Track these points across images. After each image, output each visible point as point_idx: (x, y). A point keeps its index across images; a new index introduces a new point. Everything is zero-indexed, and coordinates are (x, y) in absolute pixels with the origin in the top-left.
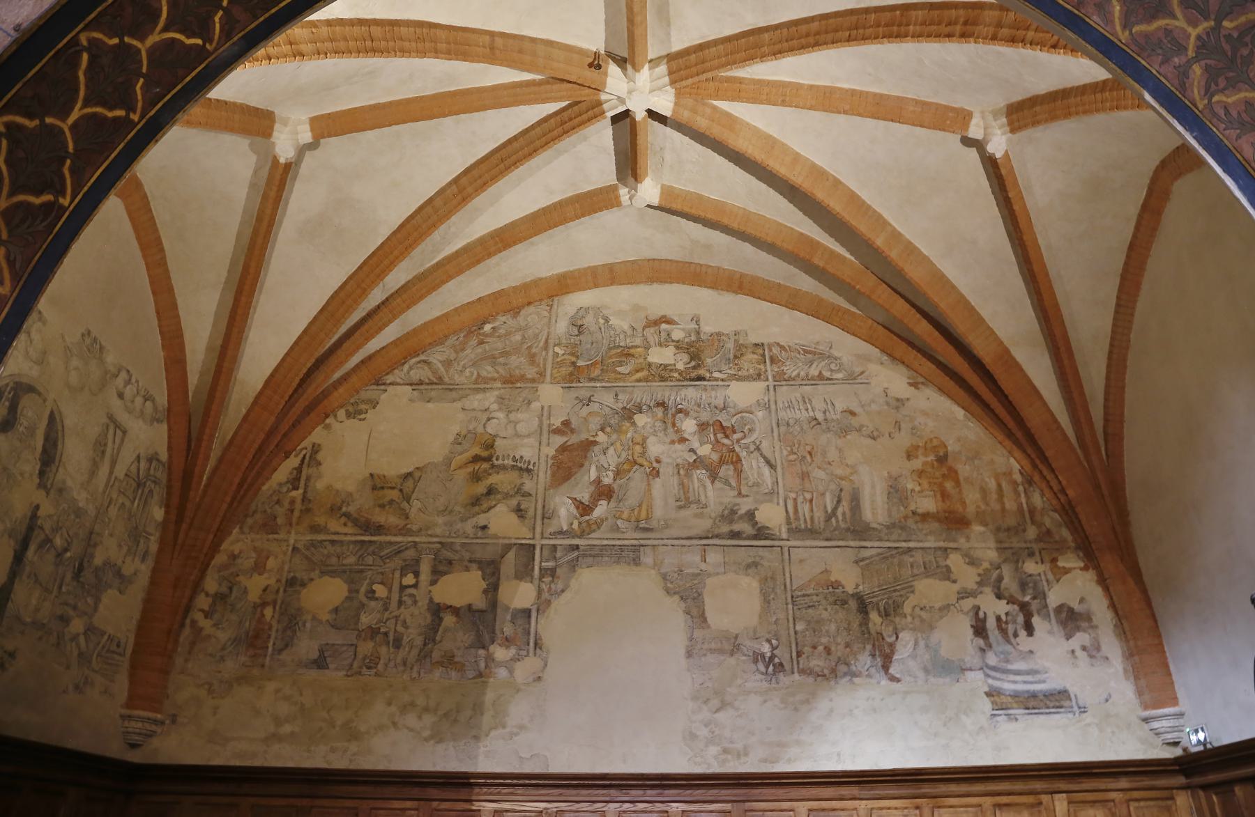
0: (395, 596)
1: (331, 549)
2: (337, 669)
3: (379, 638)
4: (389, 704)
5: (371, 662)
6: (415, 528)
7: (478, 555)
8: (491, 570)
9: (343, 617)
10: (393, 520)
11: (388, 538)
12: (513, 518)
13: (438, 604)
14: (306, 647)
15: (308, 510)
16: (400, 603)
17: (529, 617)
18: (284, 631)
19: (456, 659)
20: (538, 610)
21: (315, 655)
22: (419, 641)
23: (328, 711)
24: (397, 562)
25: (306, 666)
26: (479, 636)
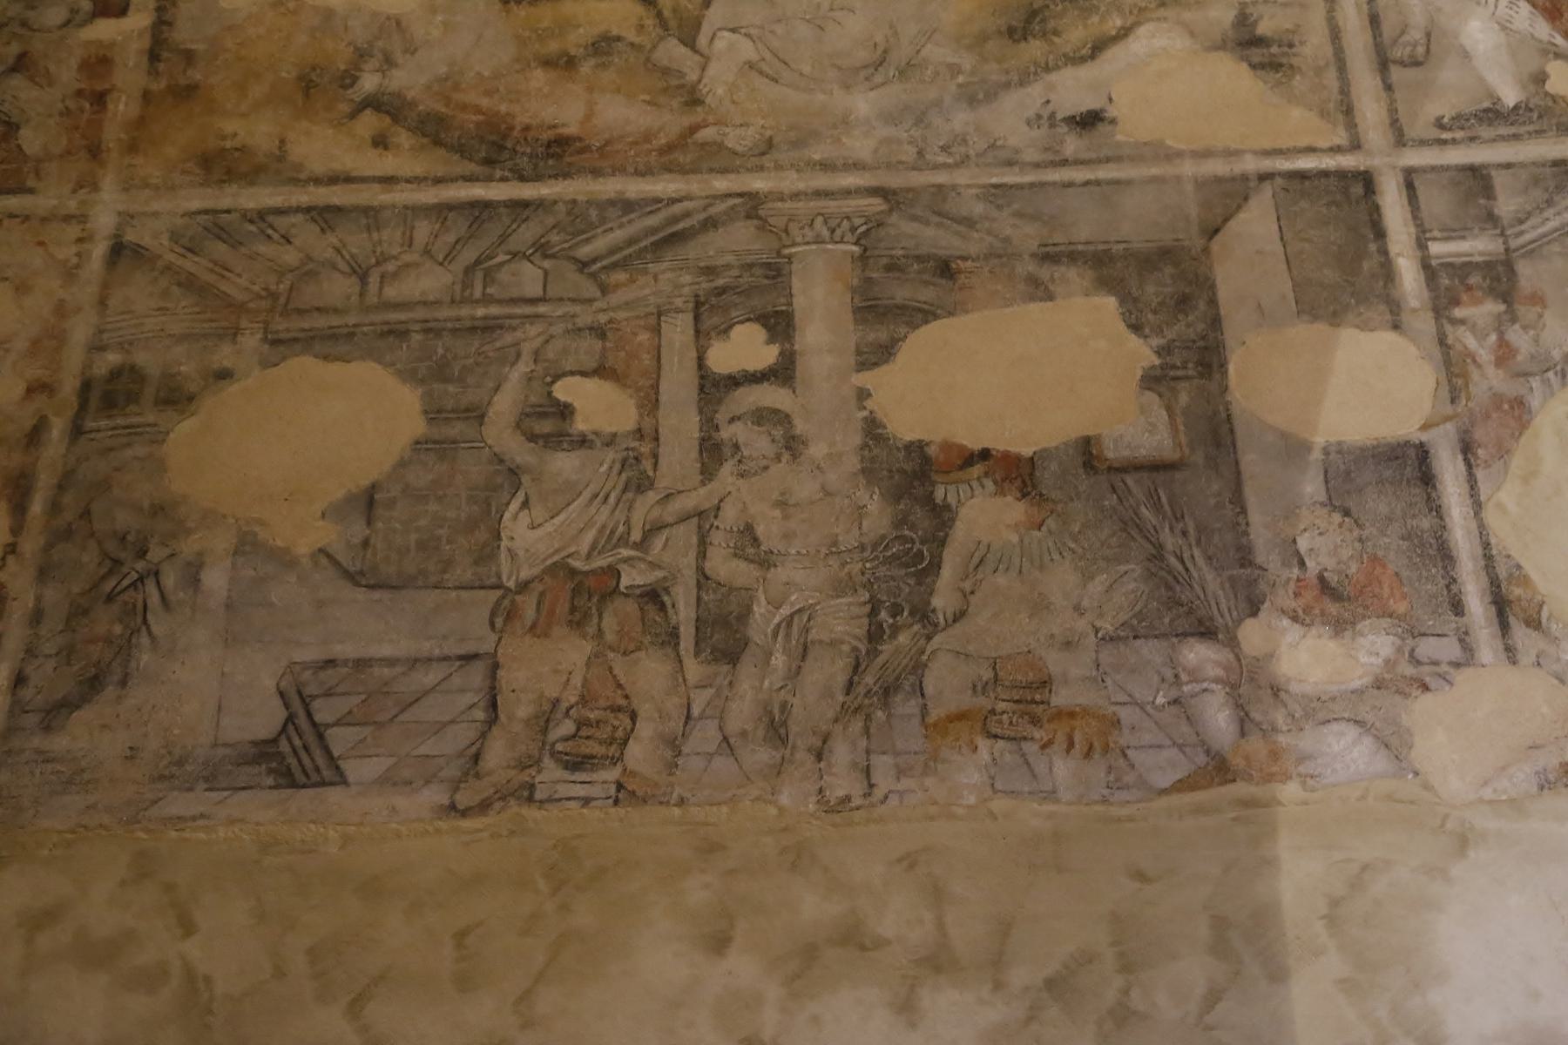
0: (680, 423)
1: (320, 244)
2: (387, 781)
3: (615, 618)
4: (719, 944)
5: (588, 738)
6: (736, 139)
7: (1086, 225)
8: (1171, 292)
9: (383, 542)
10: (619, 112)
11: (608, 187)
12: (1233, 77)
13: (917, 449)
14: (206, 682)
15: (185, 93)
16: (712, 452)
17: (1428, 479)
18: (78, 612)
19: (1061, 698)
20: (1467, 448)
21: (264, 719)
22: (841, 621)
23: (355, 1008)
24: (670, 280)
25: (211, 778)
26: (1166, 578)
